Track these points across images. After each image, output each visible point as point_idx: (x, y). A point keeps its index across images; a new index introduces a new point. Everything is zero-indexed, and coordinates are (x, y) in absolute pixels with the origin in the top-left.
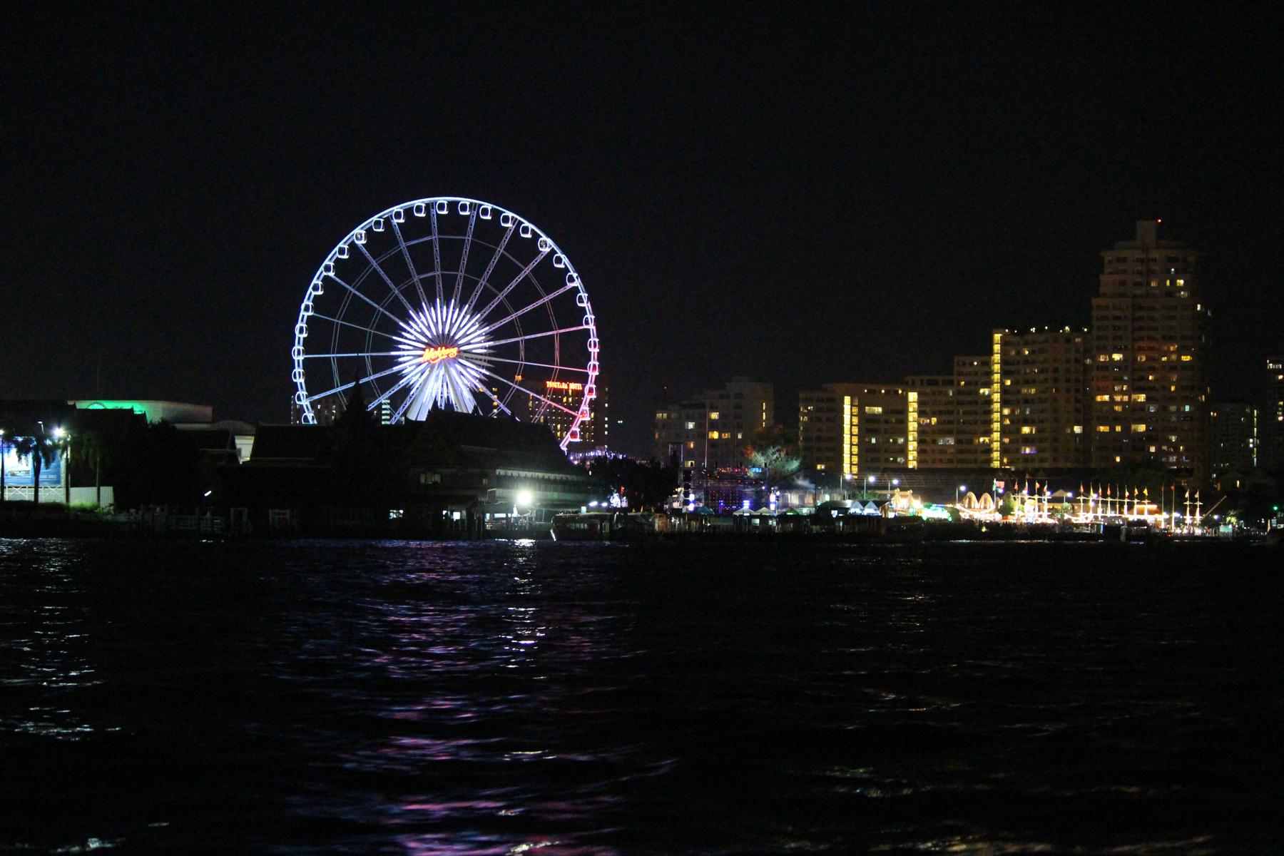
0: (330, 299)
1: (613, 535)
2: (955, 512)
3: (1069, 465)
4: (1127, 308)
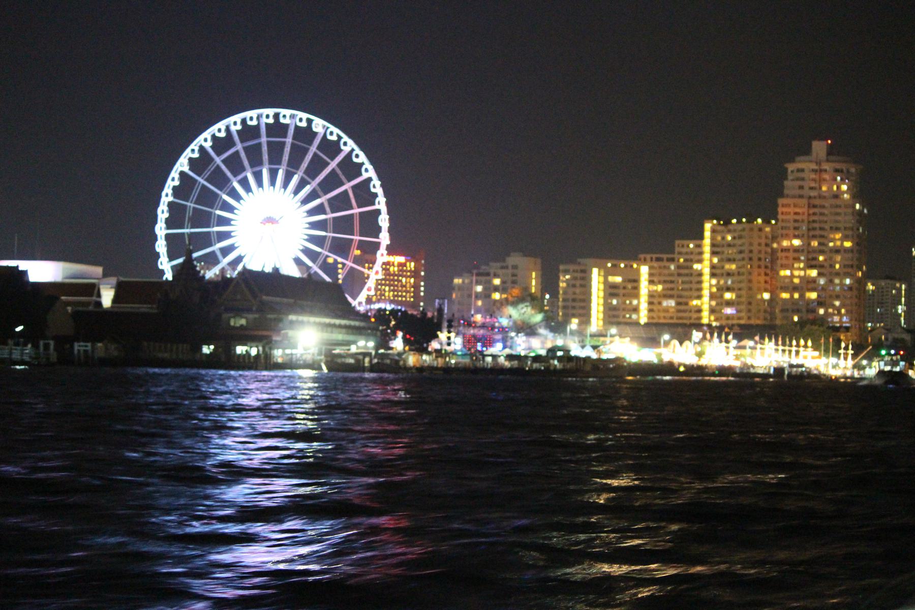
0: (185, 187)
1: (372, 369)
2: (659, 355)
3: (759, 322)
4: (804, 205)
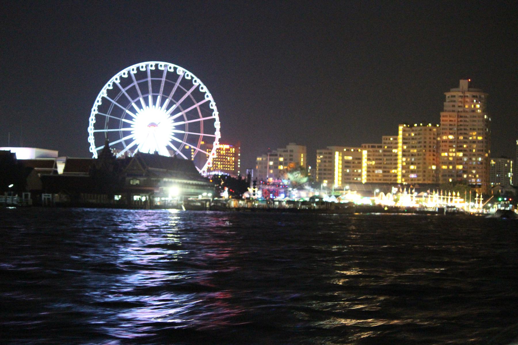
0: (105, 106)
1: (211, 208)
2: (373, 201)
3: (430, 182)
4: (455, 116)
